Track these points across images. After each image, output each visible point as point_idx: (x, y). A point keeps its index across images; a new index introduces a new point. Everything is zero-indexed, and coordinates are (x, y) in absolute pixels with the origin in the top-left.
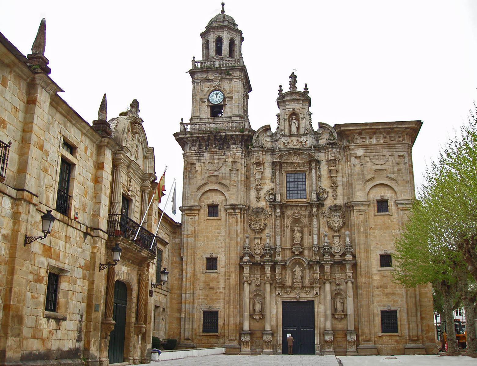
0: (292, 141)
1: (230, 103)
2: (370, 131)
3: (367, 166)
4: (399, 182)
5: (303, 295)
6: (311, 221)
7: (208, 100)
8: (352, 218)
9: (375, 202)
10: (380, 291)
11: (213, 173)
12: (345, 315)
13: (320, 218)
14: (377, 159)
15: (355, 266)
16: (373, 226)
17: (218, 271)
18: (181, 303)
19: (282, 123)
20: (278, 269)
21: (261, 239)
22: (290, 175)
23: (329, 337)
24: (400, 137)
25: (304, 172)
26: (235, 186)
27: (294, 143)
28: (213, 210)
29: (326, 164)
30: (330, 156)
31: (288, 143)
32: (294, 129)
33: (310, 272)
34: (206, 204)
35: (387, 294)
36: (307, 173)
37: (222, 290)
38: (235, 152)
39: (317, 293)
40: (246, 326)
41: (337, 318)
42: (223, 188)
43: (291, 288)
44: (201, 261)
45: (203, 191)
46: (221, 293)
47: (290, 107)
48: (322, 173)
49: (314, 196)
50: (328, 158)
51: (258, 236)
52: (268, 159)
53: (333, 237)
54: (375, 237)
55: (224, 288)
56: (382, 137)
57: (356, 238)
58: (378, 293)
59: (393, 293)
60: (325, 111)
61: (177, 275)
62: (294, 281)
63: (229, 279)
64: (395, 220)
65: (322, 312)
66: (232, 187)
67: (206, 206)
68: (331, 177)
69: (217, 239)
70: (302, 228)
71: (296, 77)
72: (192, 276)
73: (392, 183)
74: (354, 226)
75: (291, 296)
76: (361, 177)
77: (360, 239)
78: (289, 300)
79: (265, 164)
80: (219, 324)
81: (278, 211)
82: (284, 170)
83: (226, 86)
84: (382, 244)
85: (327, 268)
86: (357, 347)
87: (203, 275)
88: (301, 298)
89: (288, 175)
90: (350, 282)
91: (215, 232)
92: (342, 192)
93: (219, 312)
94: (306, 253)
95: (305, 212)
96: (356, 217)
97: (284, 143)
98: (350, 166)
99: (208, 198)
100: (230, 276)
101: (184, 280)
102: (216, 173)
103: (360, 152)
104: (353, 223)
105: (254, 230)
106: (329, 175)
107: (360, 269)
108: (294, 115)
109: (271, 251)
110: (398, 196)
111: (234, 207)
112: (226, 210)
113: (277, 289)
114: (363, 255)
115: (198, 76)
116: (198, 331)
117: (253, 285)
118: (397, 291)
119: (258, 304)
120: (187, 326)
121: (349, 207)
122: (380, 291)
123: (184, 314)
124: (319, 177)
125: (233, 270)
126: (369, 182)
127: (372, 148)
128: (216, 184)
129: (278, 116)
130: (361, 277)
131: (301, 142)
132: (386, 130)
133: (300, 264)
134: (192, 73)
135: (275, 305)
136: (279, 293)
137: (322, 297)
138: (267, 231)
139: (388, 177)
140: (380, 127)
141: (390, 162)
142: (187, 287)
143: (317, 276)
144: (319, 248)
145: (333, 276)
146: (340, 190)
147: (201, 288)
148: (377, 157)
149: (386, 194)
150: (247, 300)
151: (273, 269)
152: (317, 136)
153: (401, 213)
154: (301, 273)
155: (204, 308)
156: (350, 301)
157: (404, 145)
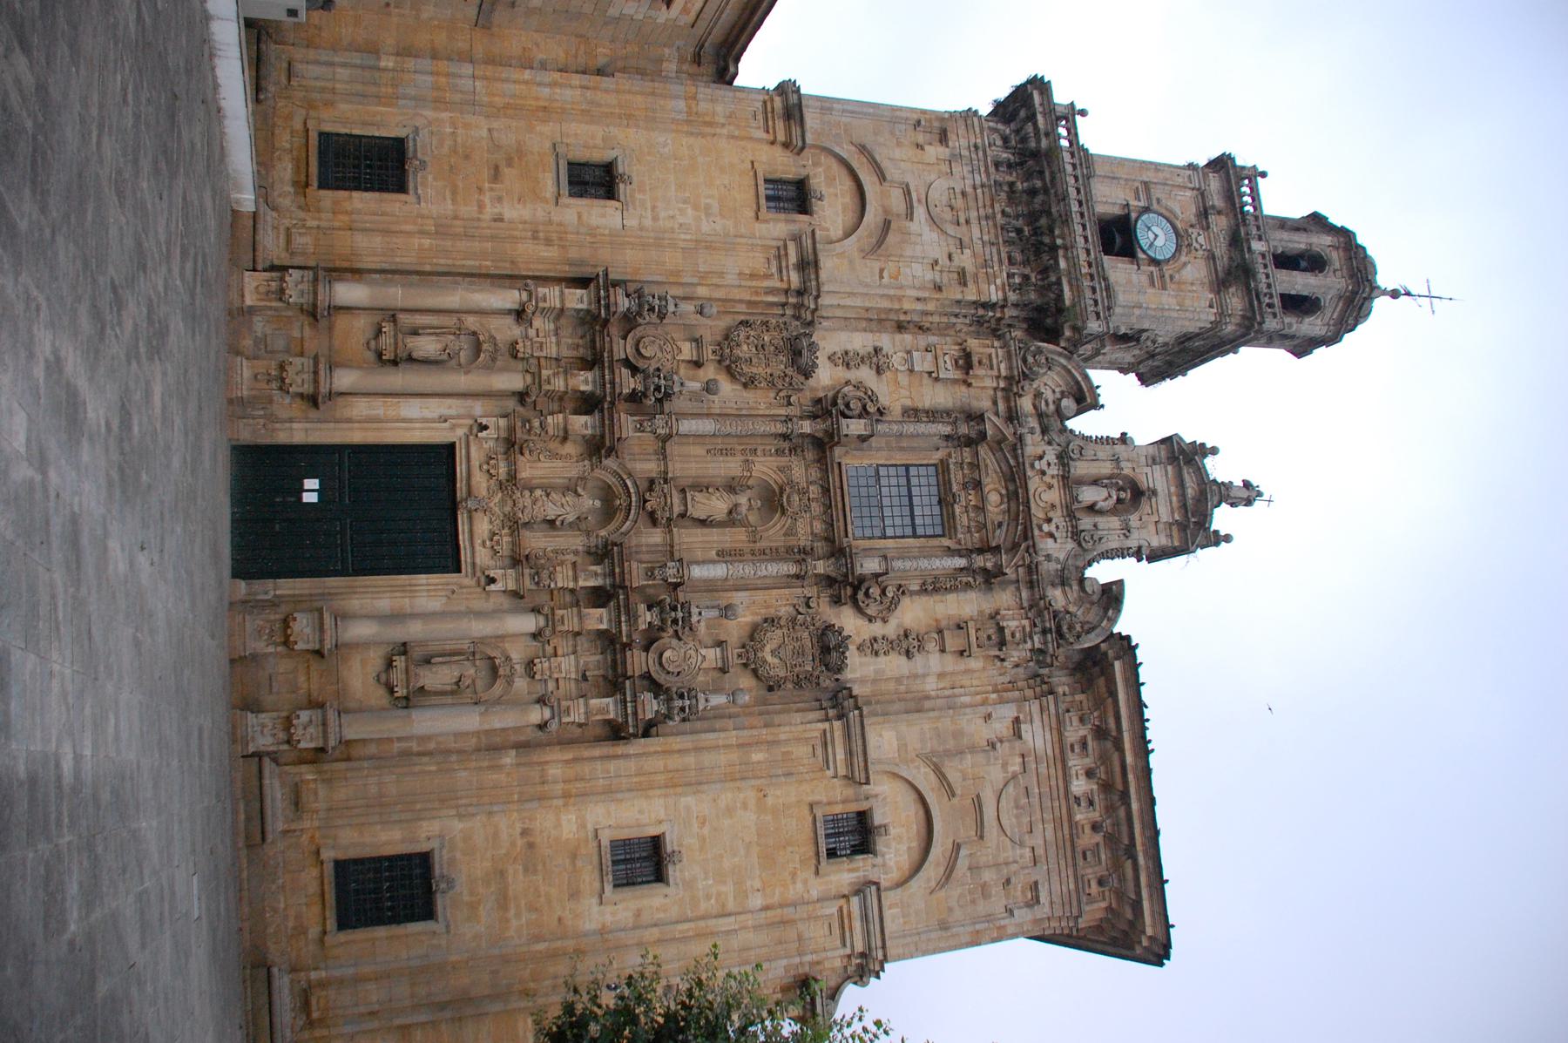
0: (1050, 487)
1: (1144, 279)
2: (1117, 769)
3: (988, 763)
4: (942, 894)
5: (483, 526)
6: (774, 555)
7: (1147, 210)
8: (798, 717)
9: (863, 806)
10: (513, 844)
11: (919, 201)
12: (407, 698)
13: (786, 591)
14: (1016, 801)
15: (616, 732)
16: (770, 801)
17: (565, 200)
18: (435, 57)
19: (1104, 452)
20: (582, 424)
21: (697, 364)
22: (933, 481)
23: (308, 630)
24: (1101, 883)
25: (948, 525)
26: (881, 277)
27: (1045, 494)
28: (795, 196)
29: (981, 613)
31: (1043, 473)
32: (1088, 495)
33: (576, 553)
34: (810, 171)
35: (502, 873)
36: (946, 542)
37: (490, 211)
38: (998, 281)
39: (492, 580)
40: (348, 293)
41: (389, 664)
42: (870, 236)
43: (512, 477)
44: (599, 142)
45: (855, 165)
46: (481, 206)
47: (1158, 479)
48: (951, 597)
49: (870, 566)
50: (1003, 618)
51: (708, 353)
52: (982, 393)
53: (720, 644)
54: (730, 811)
55: (499, 219)
56: (1095, 815)
57: (722, 735)
58: (504, 836)
59: (505, 897)
60: (1159, 604)
61: (541, 56)
62: (538, 492)
63: (535, 238)
64: (799, 886)
65: (419, 603)
66: (877, 265)
67: (803, 173)
68: (940, 632)
69: (685, 202)
70: (744, 523)
71: (1249, 502)
72: (542, 104)
73: (938, 865)
74: (766, 726)
75: (476, 473)
76: (951, 744)
77: (717, 749)
78: (461, 469)
79: (964, 388)
80: (356, 194)
81: (807, 427)
82: (950, 455)
83: (1194, 271)
84: (703, 839)
85: (598, 619)
86: (268, 754)
87: (548, 145)
88: (470, 518)
89: (932, 470)
90: (547, 713)
91: (709, 197)
92: (889, 674)
93: (402, 197)
94: (656, 537)
95: (807, 528)
96: (801, 728)
97: (1041, 458)
98: (984, 703)
99: (831, 180)
100: (548, 242)
101: (527, 75)
102: (920, 212)
103: (1037, 736)
104: (777, 719)
105: (727, 337)
106: (943, 624)
107: (601, 758)
108: (1134, 495)
109: (653, 398)
110: (891, 894)
111: (808, 265)
112: (797, 238)
113: (503, 422)
114: (658, 763)
115: (1214, 183)
116: (325, 114)
117: (516, 331)
118: (518, 915)
119: (439, 346)
120: (343, 73)
121: (840, 703)
122: (513, 844)
123: (391, 65)
124: (933, 586)
125: (573, 254)
126: (932, 777)
127: (1053, 783)
128: (880, 210)
129: (1124, 438)
130: (567, 762)
131: (1049, 520)
132: (1124, 829)
133: (609, 511)
134: (1222, 164)
135: (435, 415)
136: (486, 428)
137: (478, 604)
138: (726, 387)
139: (957, 847)
140: (1135, 806)
141: (1010, 853)
142: (498, 85)
143: (563, 579)
144: (676, 586)
145: (564, 646)
146: (894, 664)
147: (495, 134)
148: (1024, 801)
149: (893, 844)
150: (454, 298)
151: (588, 404)
152: (1071, 576)
153: (832, 909)
154: (571, 518)
155: (424, 148)
156: (468, 721)
157: (1075, 903)
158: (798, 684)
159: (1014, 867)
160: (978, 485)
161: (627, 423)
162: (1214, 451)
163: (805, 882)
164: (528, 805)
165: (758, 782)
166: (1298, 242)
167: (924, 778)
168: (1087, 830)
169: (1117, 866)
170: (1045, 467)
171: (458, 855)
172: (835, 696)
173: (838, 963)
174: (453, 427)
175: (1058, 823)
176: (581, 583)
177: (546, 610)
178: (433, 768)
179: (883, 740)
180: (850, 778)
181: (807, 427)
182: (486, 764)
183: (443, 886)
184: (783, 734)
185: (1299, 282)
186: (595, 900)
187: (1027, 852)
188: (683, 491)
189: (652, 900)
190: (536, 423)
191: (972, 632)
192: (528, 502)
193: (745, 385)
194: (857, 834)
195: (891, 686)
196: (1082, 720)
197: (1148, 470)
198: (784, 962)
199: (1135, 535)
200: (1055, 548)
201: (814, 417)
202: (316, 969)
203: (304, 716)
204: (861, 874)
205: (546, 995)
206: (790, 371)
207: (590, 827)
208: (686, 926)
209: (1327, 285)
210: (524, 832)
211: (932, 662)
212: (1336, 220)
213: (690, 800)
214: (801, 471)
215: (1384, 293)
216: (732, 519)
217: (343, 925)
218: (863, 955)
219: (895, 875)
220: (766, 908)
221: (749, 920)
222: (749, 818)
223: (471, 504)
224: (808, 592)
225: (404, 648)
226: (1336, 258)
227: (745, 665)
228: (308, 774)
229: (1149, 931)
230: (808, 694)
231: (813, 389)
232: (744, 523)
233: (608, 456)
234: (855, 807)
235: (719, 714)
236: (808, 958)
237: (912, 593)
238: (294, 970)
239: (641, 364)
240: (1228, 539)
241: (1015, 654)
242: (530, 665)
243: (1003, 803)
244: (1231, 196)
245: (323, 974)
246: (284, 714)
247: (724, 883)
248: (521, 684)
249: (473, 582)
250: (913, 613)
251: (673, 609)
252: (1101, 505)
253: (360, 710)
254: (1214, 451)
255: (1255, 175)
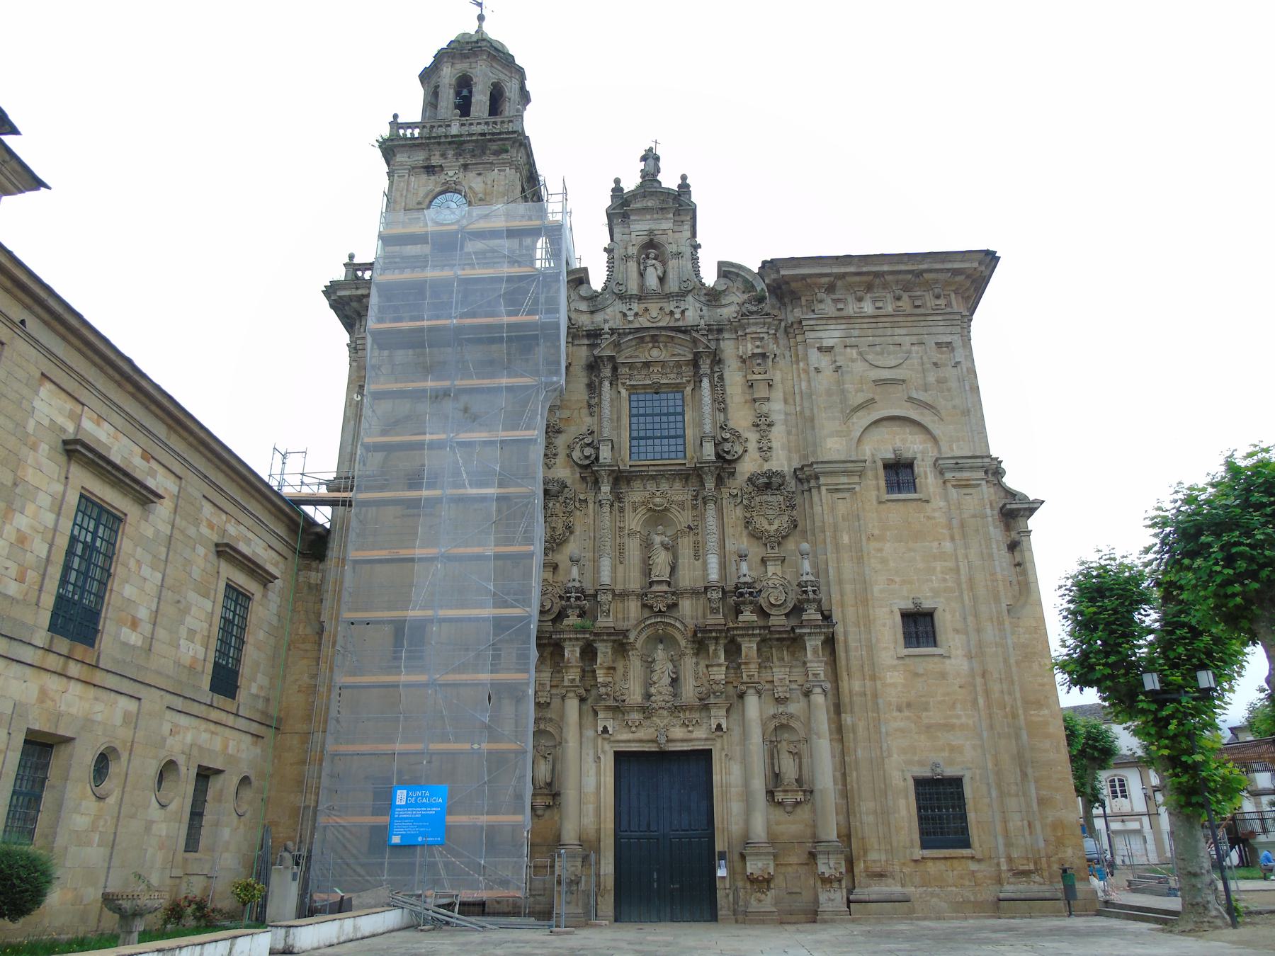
0: (646, 310)
2: (857, 279)
4: (943, 413)
5: (678, 732)
8: (817, 509)
10: (908, 718)
14: (878, 354)
16: (876, 532)
24: (938, 297)
27: (654, 315)
29: (740, 369)
30: (749, 346)
31: (636, 314)
32: (652, 281)
33: (697, 664)
35: (929, 727)
39: (719, 727)
41: (780, 804)
47: (640, 227)
48: (729, 390)
49: (709, 450)
53: (764, 561)
56: (889, 297)
58: (902, 724)
59: (946, 725)
60: (732, 236)
61: (306, 678)
62: (653, 690)
64: (936, 514)
68: (755, 400)
71: (657, 159)
75: (636, 737)
78: (635, 747)
81: (606, 488)
84: (904, 582)
85: (749, 648)
94: (686, 606)
95: (680, 493)
97: (625, 315)
98: (806, 372)
103: (832, 335)
104: (818, 524)
106: (748, 397)
108: (651, 245)
113: (601, 715)
114: (850, 611)
118: (958, 717)
121: (807, 477)
122: (908, 718)
124: (720, 404)
131: (672, 313)
132: (900, 277)
133: (662, 639)
135: (594, 766)
139: (910, 399)
140: (886, 268)
143: (719, 674)
146: (778, 436)
148: (878, 348)
151: (589, 653)
152: (713, 296)
156: (824, 748)
158: (793, 507)
159: (925, 358)
160: (647, 365)
161: (603, 622)
162: (617, 181)
163: (934, 510)
164: (881, 706)
165: (864, 538)
166: (448, 97)
167: (864, 419)
168: (900, 304)
169: (928, 286)
170: (632, 313)
171: (916, 758)
172: (800, 480)
173: (992, 490)
174: (603, 752)
175: (895, 325)
176: (722, 660)
177: (743, 688)
178: (854, 774)
179: (834, 447)
180: (861, 474)
181: (606, 488)
182: (851, 735)
183: (939, 770)
184: (829, 519)
185: (480, 99)
186: (947, 661)
187: (915, 348)
188: (651, 584)
189: (946, 621)
190: (602, 690)
191: (755, 377)
192: (659, 698)
193: (571, 533)
194: (899, 473)
195: (792, 438)
196: (821, 301)
197: (634, 234)
198: (991, 528)
199: (682, 249)
200: (692, 313)
201: (596, 483)
202: (998, 864)
203: (822, 868)
204: (928, 470)
205: (1015, 699)
206: (561, 499)
207: (895, 662)
208: (966, 597)
209: (483, 77)
210: (900, 710)
211: (776, 408)
212: (428, 61)
213: (876, 589)
214: (636, 494)
215: (480, 26)
216: (670, 548)
217: (967, 844)
218: (986, 472)
219: (929, 445)
220: (952, 539)
221: (961, 552)
222: (888, 547)
223: (663, 740)
224: (726, 495)
225: (770, 793)
226: (462, 66)
227: (779, 544)
228: (859, 867)
229: (975, 265)
230: (798, 500)
231: (573, 483)
232: (675, 538)
233: (627, 637)
234: (881, 472)
235: (815, 565)
236: (989, 511)
237: (726, 419)
238: (999, 881)
239: (556, 610)
240: (684, 178)
241: (771, 346)
242: (779, 701)
243: (879, 363)
244: (413, 145)
245: (1002, 860)
246: (819, 883)
247: (935, 568)
248: (793, 708)
249: (719, 740)
250: (741, 418)
251: (738, 596)
252: (660, 273)
253: (815, 826)
254: (617, 181)
255: (395, 124)
